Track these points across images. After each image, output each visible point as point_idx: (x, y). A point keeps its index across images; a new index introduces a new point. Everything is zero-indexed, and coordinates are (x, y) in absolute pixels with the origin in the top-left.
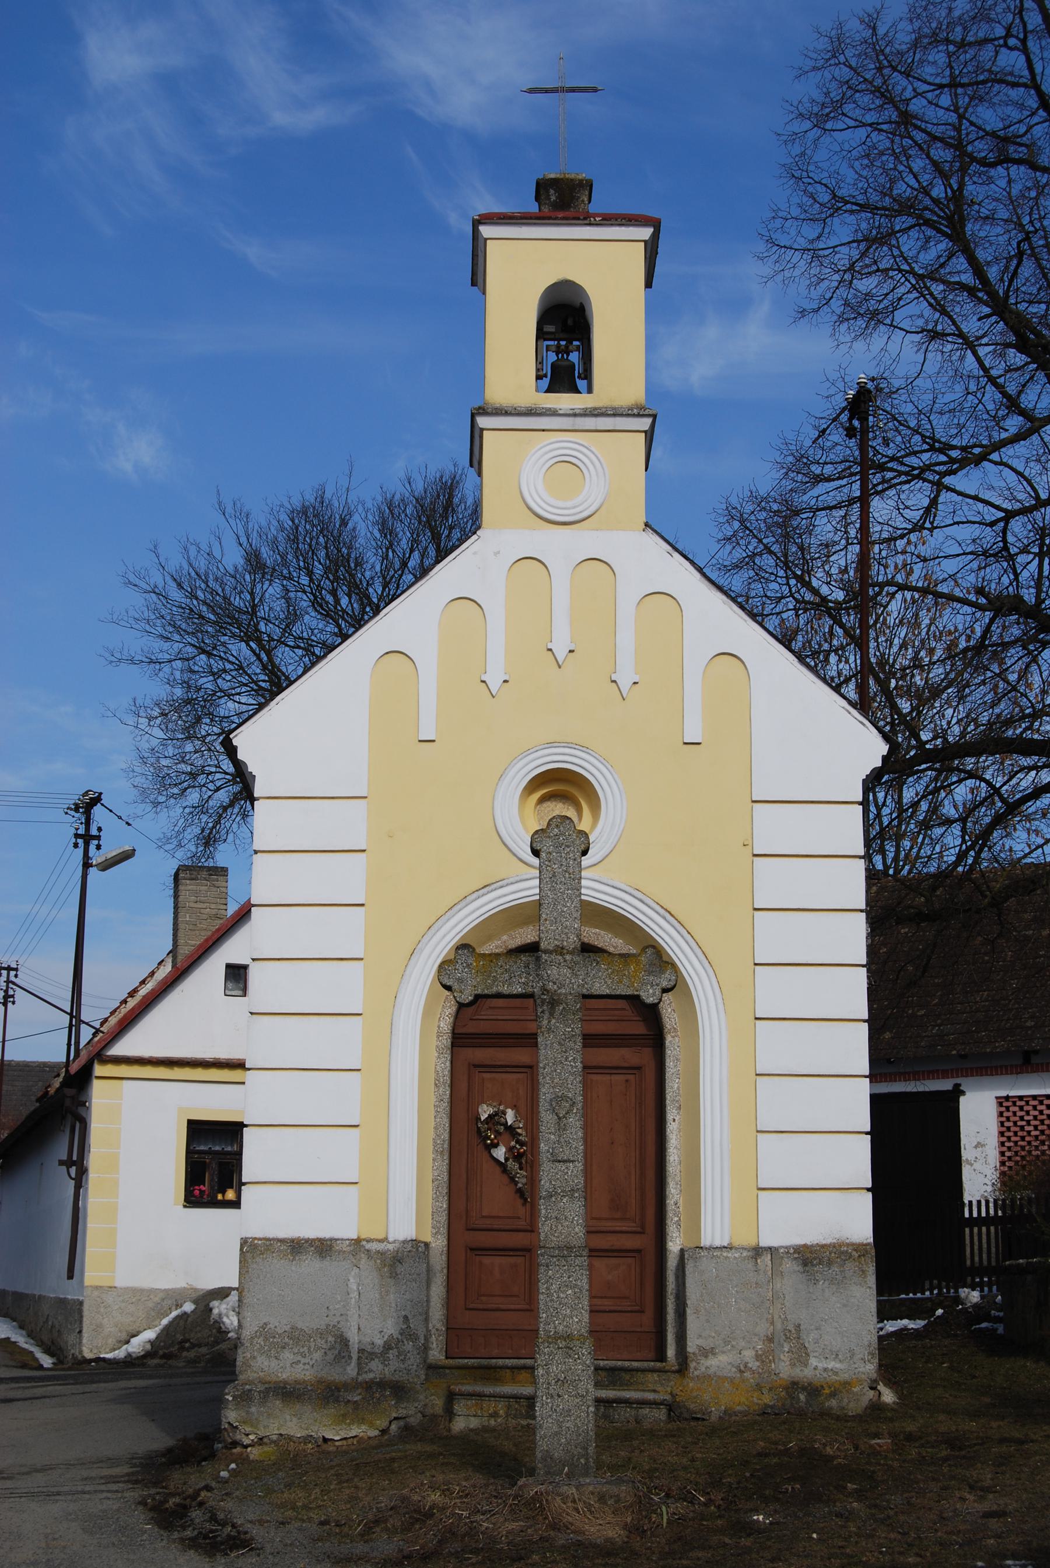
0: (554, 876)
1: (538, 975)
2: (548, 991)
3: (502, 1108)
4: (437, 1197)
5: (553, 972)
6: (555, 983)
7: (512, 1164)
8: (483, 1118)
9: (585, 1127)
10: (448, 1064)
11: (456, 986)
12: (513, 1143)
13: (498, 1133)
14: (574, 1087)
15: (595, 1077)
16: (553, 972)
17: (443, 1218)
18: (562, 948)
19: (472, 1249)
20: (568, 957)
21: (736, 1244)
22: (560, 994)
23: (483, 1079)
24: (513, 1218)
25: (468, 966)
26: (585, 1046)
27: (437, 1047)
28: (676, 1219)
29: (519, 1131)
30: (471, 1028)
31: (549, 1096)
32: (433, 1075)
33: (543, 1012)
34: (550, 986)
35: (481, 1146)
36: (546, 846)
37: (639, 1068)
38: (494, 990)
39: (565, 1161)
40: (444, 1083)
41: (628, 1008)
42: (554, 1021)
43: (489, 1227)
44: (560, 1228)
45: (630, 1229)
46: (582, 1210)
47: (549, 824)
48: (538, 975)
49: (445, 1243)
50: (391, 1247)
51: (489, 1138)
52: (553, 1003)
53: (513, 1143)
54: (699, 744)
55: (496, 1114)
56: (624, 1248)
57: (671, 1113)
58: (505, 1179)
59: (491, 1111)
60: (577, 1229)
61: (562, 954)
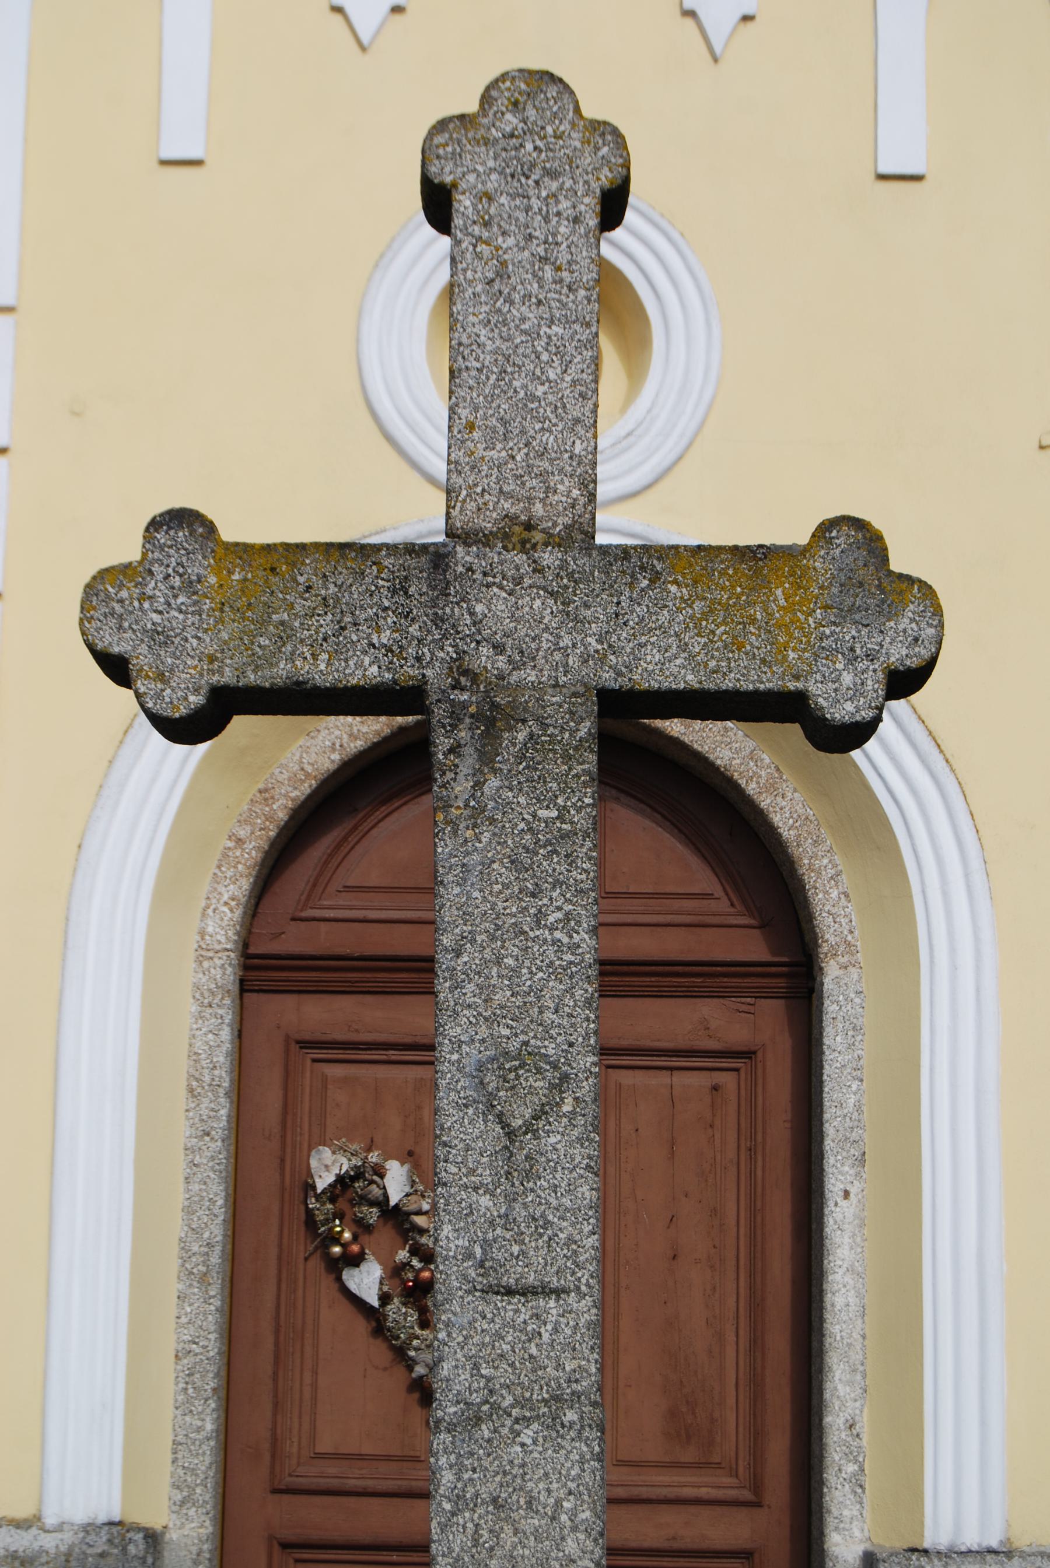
0: (502, 273)
1: (438, 620)
2: (475, 678)
3: (374, 1157)
4: (189, 1401)
5: (494, 608)
6: (499, 648)
7: (398, 1313)
8: (321, 1185)
9: (603, 1170)
10: (226, 1034)
11: (142, 658)
12: (403, 1255)
13: (362, 1228)
14: (568, 1019)
15: (627, 1078)
16: (494, 608)
17: (204, 1459)
18: (529, 526)
19: (285, 1546)
20: (549, 558)
21: (1022, 1542)
22: (519, 686)
23: (325, 1080)
24: (403, 1459)
25: (190, 586)
26: (605, 992)
27: (197, 987)
28: (851, 1468)
29: (420, 1221)
30: (294, 941)
31: (472, 1054)
32: (183, 1066)
33: (454, 750)
34: (484, 658)
35: (316, 1264)
36: (472, 175)
37: (748, 1054)
38: (280, 672)
39: (527, 1292)
40: (213, 1087)
41: (719, 892)
42: (493, 783)
43: (335, 1483)
44: (508, 1537)
45: (720, 1494)
46: (591, 1476)
47: (486, 99)
48: (438, 620)
49: (208, 1528)
50: (49, 1542)
51: (336, 1240)
52: (493, 719)
53: (403, 1255)
54: (917, 178)
55: (358, 1174)
56: (705, 1545)
57: (838, 1174)
58: (380, 1352)
59: (343, 1164)
60: (571, 1546)
61: (525, 546)
